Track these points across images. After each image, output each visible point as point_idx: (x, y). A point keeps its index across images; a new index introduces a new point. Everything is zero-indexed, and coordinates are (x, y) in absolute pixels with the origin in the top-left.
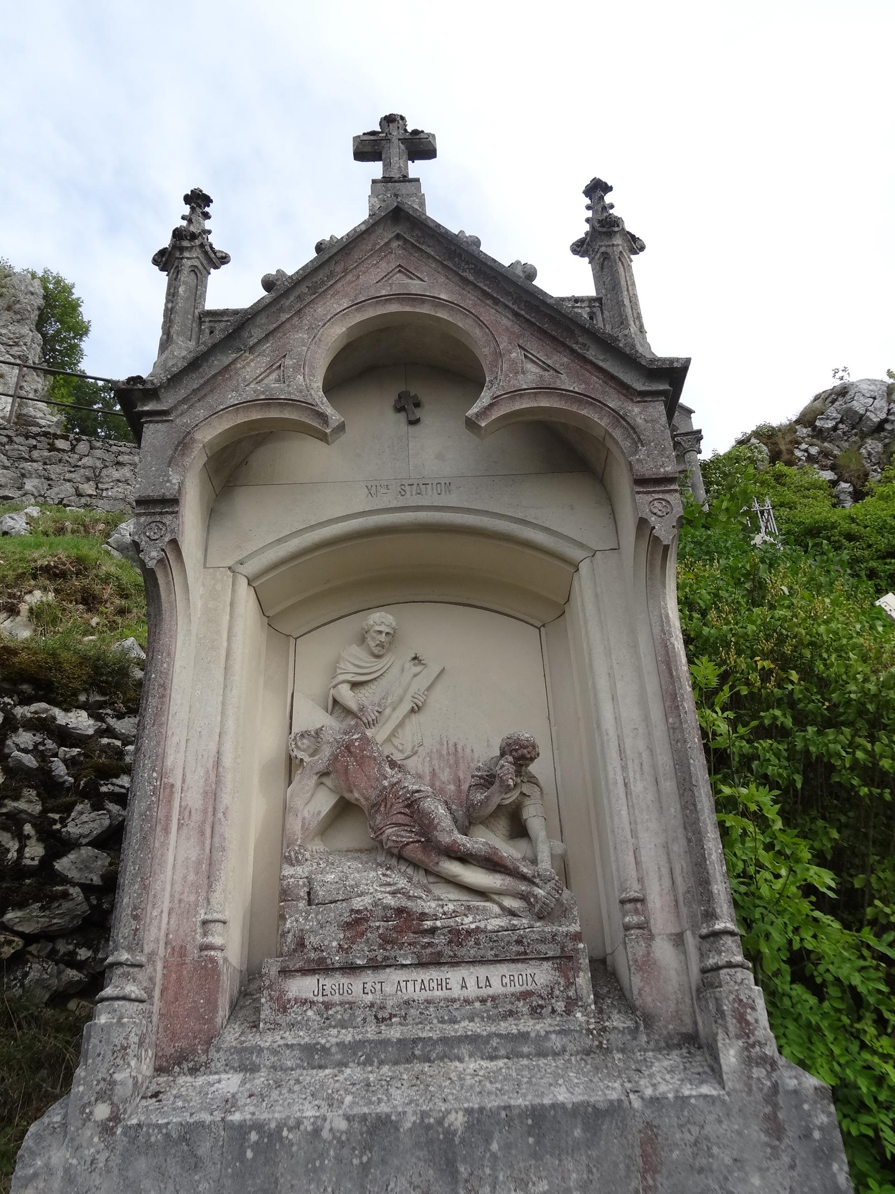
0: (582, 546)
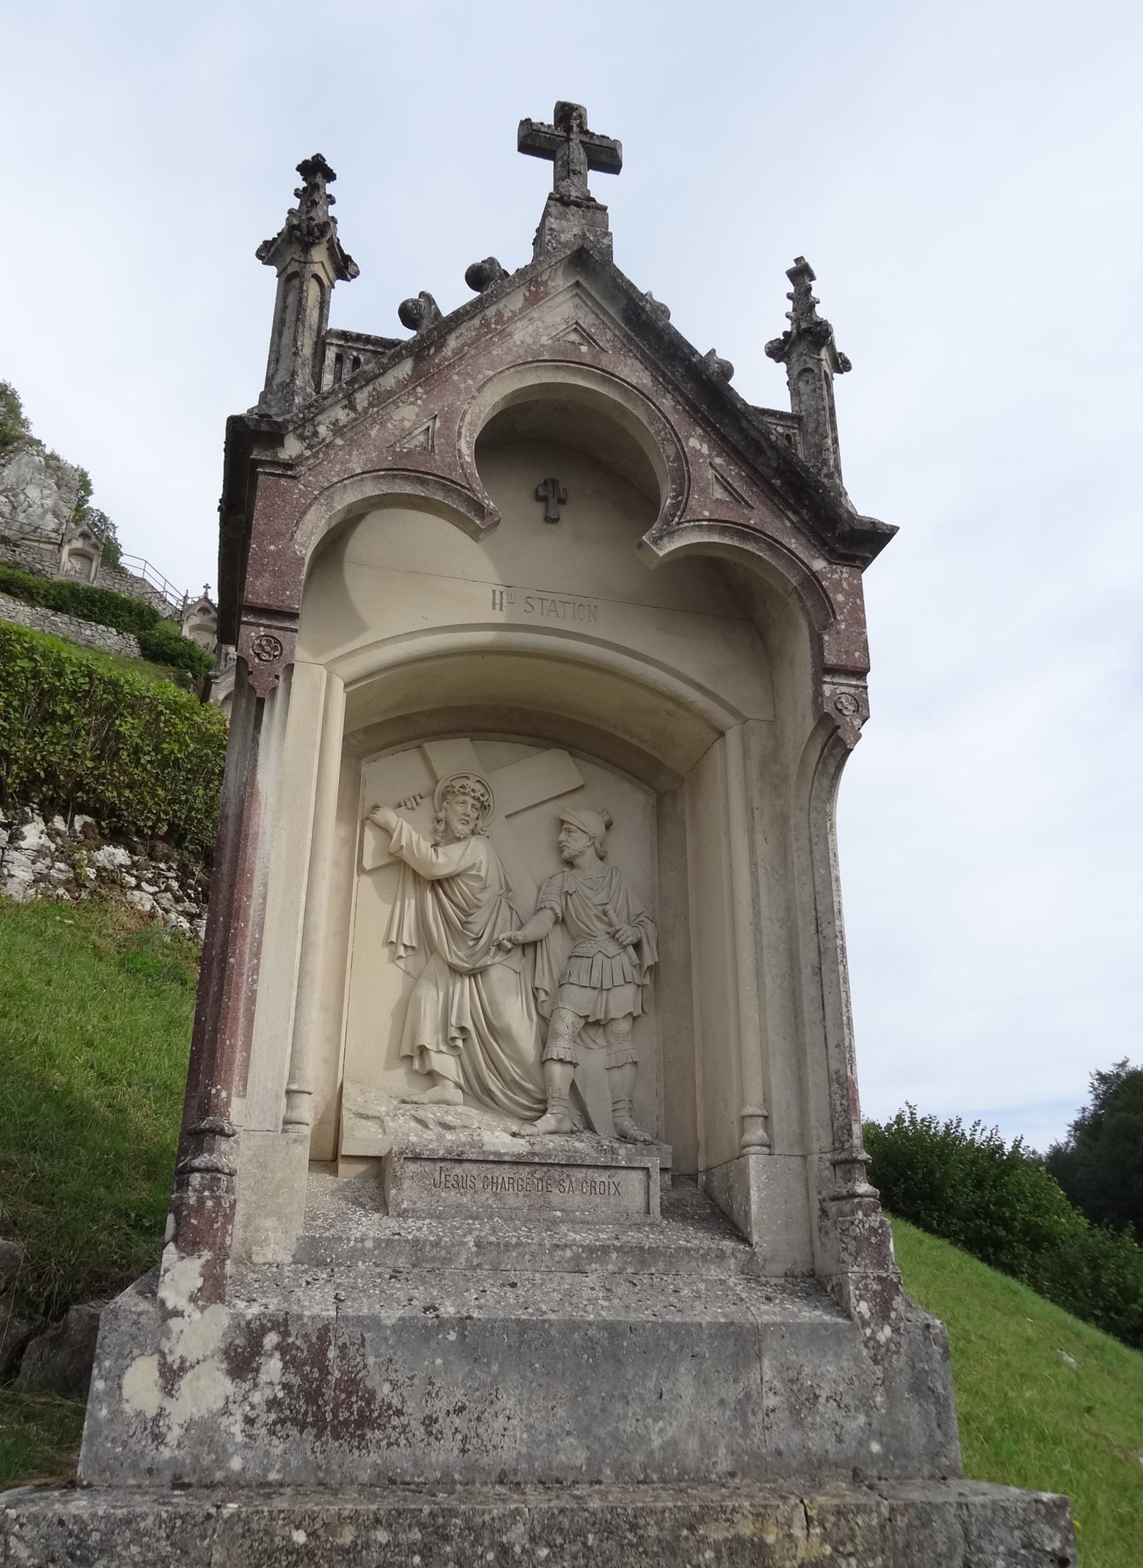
0: (735, 713)
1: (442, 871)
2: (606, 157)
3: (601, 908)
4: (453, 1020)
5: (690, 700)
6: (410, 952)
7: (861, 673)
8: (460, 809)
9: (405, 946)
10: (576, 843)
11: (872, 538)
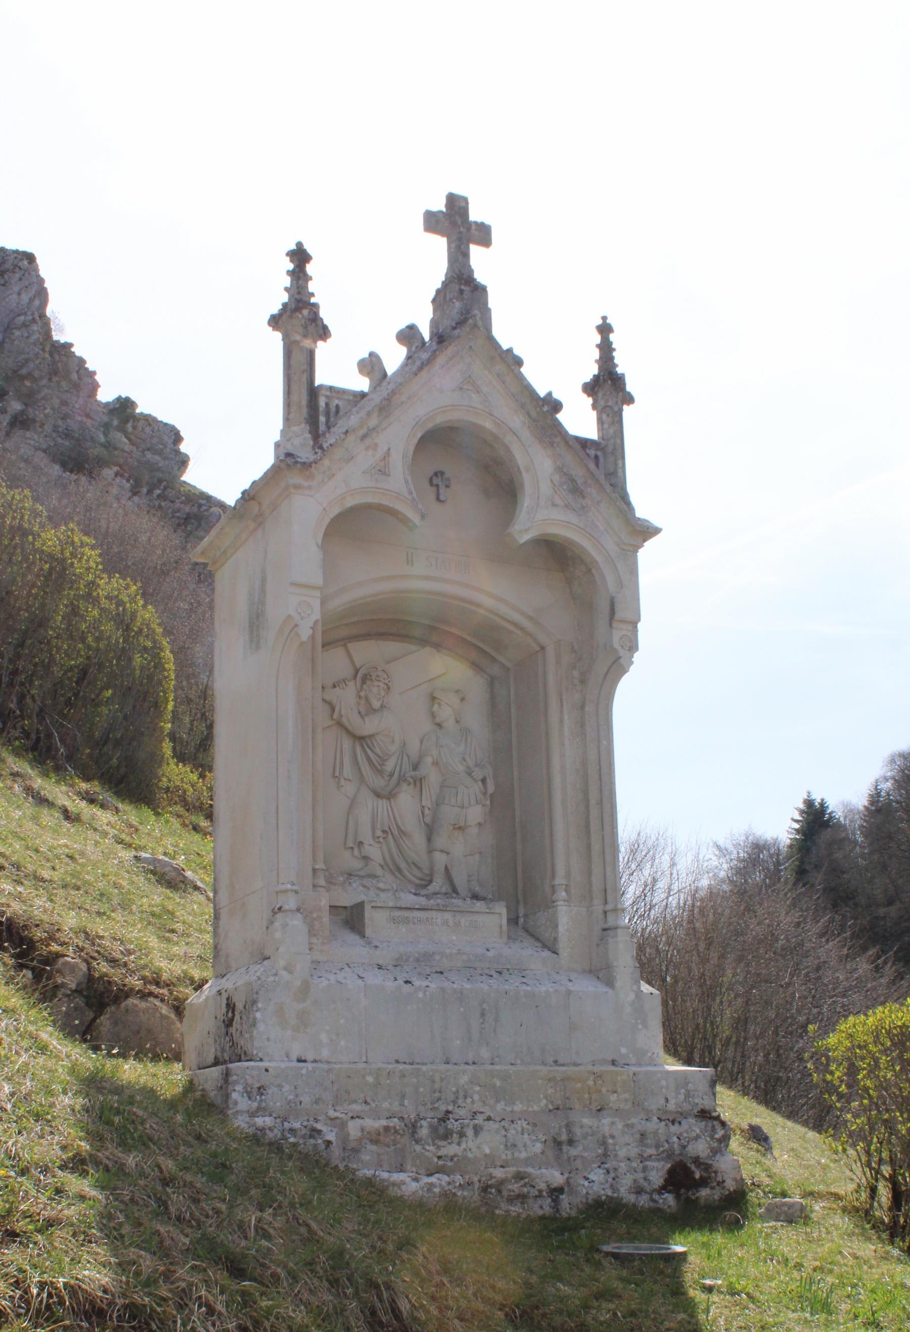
1: (366, 733)
2: (483, 235)
11: (646, 532)
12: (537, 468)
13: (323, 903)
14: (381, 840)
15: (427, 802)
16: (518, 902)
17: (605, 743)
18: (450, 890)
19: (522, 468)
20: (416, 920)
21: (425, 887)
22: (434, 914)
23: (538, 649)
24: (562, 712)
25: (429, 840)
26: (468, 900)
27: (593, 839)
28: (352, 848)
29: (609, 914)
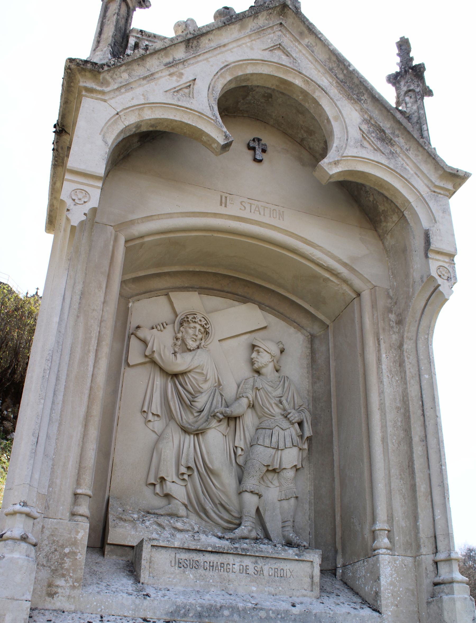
3: (278, 399)
4: (183, 462)
5: (339, 272)
6: (156, 418)
7: (451, 256)
8: (191, 331)
9: (153, 414)
10: (263, 359)
11: (457, 178)
12: (346, 123)
13: (79, 536)
14: (186, 477)
15: (240, 443)
16: (336, 551)
17: (427, 376)
18: (261, 535)
19: (331, 118)
20: (207, 565)
21: (231, 530)
22: (230, 559)
23: (354, 296)
24: (379, 351)
25: (240, 481)
26: (279, 547)
27: (418, 480)
28: (154, 485)
29: (440, 565)
